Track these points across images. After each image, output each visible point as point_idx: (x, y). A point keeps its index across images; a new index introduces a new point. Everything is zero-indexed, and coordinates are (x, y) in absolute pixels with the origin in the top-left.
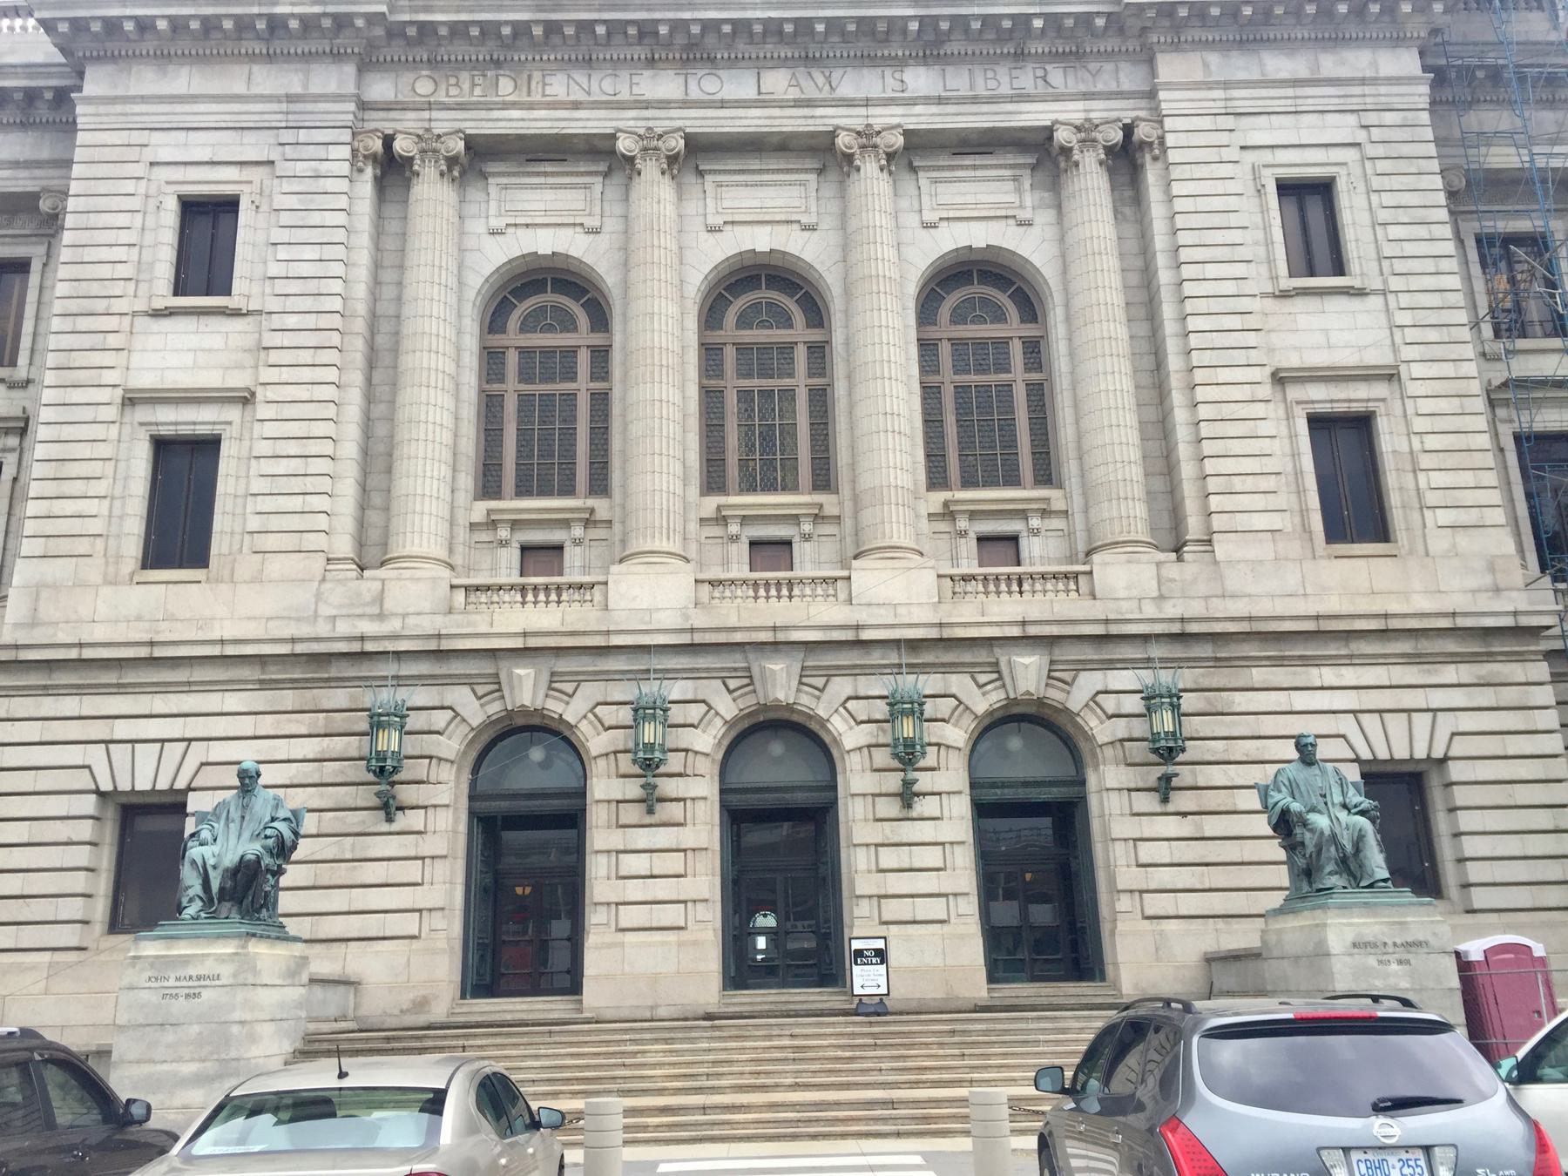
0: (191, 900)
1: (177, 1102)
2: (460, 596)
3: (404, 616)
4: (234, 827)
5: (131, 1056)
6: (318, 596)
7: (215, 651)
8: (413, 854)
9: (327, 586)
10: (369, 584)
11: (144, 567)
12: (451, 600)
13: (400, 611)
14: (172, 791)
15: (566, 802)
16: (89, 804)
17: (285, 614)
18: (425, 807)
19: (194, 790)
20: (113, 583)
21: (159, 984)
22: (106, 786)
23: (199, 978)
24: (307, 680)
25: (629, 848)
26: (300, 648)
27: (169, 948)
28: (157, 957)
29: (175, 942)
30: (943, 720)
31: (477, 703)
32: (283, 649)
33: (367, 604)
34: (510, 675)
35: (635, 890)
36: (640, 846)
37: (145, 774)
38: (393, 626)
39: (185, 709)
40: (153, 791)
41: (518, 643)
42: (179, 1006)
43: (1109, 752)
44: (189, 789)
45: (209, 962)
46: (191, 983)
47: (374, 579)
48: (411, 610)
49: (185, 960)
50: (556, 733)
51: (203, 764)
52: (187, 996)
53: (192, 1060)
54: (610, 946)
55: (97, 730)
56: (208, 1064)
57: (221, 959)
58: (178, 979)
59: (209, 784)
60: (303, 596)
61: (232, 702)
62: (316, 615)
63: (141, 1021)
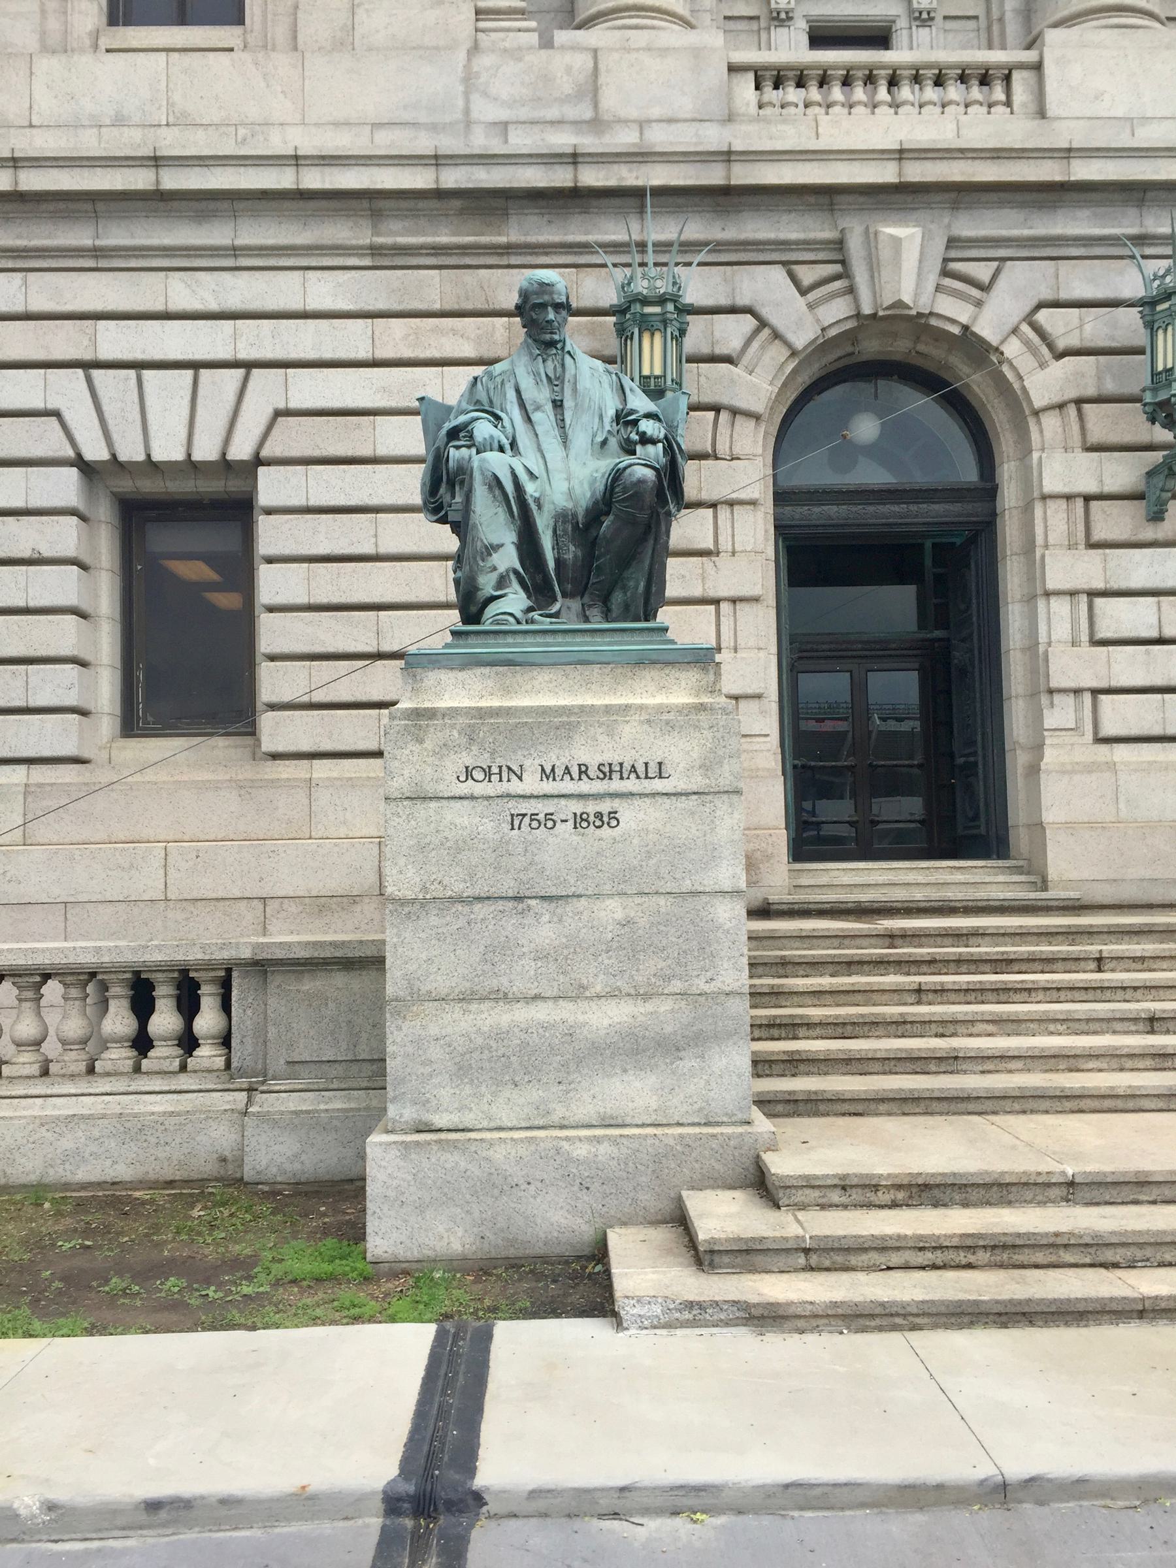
0: (502, 582)
1: (584, 1108)
2: (745, 87)
3: (642, 124)
4: (544, 419)
5: (440, 983)
6: (469, 79)
7: (283, 179)
8: (697, 592)
9: (484, 61)
10: (568, 58)
11: (113, 21)
12: (729, 96)
13: (634, 114)
14: (225, 465)
15: (956, 508)
16: (64, 486)
17: (407, 116)
18: (713, 505)
19: (269, 463)
20: (64, 48)
21: (492, 788)
22: (95, 452)
23: (607, 772)
24: (464, 249)
25: (1115, 585)
26: (452, 178)
27: (507, 691)
28: (482, 714)
29: (520, 676)
30: (728, 360)
31: (801, 302)
32: (418, 179)
33: (565, 100)
34: (871, 239)
35: (1129, 667)
36: (1136, 583)
37: (169, 428)
38: (624, 139)
39: (234, 303)
40: (191, 466)
41: (885, 174)
42: (560, 848)
43: (1051, 422)
44: (258, 461)
45: (629, 730)
46: (585, 786)
47: (575, 48)
48: (655, 112)
49: (563, 723)
50: (928, 380)
51: (278, 414)
52: (580, 820)
53: (613, 994)
54: (1091, 768)
55: (64, 341)
56: (665, 1006)
57: (663, 721)
58: (548, 774)
59: (295, 453)
60: (438, 81)
61: (324, 290)
62: (468, 123)
63: (458, 887)
